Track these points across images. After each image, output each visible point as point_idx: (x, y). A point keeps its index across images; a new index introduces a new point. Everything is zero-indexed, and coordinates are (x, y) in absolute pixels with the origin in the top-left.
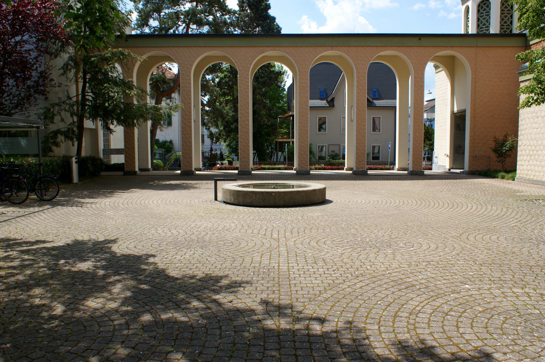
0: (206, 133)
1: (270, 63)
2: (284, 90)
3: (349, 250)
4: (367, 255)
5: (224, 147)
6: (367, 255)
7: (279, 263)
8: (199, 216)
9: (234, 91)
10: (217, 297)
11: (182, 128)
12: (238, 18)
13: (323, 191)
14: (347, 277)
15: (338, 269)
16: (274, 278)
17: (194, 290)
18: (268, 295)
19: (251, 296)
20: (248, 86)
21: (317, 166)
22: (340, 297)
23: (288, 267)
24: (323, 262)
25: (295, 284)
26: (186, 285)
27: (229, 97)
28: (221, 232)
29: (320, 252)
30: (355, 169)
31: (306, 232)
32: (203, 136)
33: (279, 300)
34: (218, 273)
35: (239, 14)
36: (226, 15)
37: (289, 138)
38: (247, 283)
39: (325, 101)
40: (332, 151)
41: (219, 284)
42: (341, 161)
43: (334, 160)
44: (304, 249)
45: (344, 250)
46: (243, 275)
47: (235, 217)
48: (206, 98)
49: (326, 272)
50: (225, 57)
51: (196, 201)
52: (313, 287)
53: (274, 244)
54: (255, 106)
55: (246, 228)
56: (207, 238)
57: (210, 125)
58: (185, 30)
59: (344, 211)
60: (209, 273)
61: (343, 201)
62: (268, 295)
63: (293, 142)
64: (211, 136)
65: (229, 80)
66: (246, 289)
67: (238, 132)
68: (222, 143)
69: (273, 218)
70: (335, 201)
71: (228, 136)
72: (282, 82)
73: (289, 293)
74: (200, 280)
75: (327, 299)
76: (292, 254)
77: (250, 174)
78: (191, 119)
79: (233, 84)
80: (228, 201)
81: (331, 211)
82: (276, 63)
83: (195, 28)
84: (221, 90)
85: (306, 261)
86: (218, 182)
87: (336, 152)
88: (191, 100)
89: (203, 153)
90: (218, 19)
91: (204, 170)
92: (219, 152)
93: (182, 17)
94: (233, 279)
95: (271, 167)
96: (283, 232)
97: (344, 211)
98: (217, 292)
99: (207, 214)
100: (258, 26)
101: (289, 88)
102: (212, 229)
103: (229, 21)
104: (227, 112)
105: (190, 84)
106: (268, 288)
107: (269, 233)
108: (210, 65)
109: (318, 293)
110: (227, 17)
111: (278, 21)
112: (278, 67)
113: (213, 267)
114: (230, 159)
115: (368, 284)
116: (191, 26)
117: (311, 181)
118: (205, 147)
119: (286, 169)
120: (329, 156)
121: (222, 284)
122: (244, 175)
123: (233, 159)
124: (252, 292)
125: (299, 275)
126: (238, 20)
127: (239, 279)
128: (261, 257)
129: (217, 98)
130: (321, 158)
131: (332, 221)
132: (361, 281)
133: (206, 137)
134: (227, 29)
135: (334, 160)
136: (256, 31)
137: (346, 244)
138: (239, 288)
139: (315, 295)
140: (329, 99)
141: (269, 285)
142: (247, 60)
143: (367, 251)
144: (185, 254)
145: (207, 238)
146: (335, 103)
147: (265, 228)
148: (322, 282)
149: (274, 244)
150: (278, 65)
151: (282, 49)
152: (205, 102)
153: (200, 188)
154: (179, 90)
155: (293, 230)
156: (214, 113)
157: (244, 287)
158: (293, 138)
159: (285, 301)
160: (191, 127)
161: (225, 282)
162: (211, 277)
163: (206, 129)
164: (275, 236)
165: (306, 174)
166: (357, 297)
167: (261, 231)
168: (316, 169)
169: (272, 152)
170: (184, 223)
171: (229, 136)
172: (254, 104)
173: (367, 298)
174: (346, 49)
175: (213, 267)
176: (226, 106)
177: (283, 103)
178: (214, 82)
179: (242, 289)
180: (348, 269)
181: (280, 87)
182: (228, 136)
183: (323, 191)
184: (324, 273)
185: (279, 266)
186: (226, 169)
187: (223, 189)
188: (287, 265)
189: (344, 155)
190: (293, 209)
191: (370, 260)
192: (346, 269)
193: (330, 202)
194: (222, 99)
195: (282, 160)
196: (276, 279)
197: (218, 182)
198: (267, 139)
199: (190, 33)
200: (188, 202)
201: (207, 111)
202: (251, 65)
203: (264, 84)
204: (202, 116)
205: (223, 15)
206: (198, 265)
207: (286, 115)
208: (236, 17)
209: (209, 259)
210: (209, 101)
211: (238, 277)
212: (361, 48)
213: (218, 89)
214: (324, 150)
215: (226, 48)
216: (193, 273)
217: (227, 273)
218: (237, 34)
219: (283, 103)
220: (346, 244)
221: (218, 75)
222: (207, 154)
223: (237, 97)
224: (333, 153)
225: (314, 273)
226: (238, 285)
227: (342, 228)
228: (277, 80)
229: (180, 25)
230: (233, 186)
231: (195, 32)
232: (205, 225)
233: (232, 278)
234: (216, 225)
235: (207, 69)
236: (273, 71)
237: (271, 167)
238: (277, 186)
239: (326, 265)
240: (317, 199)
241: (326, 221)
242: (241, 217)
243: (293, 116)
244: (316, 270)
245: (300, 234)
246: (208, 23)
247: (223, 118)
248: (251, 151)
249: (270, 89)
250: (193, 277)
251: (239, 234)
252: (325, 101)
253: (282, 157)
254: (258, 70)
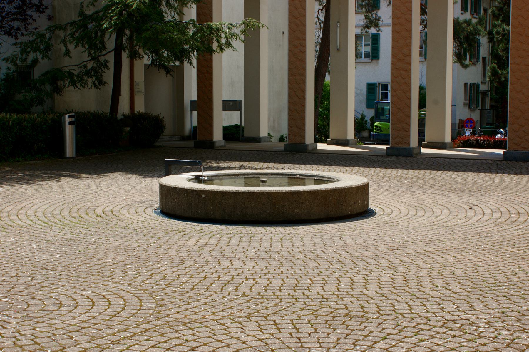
13: (362, 191)
183: (362, 191)
240: (350, 206)
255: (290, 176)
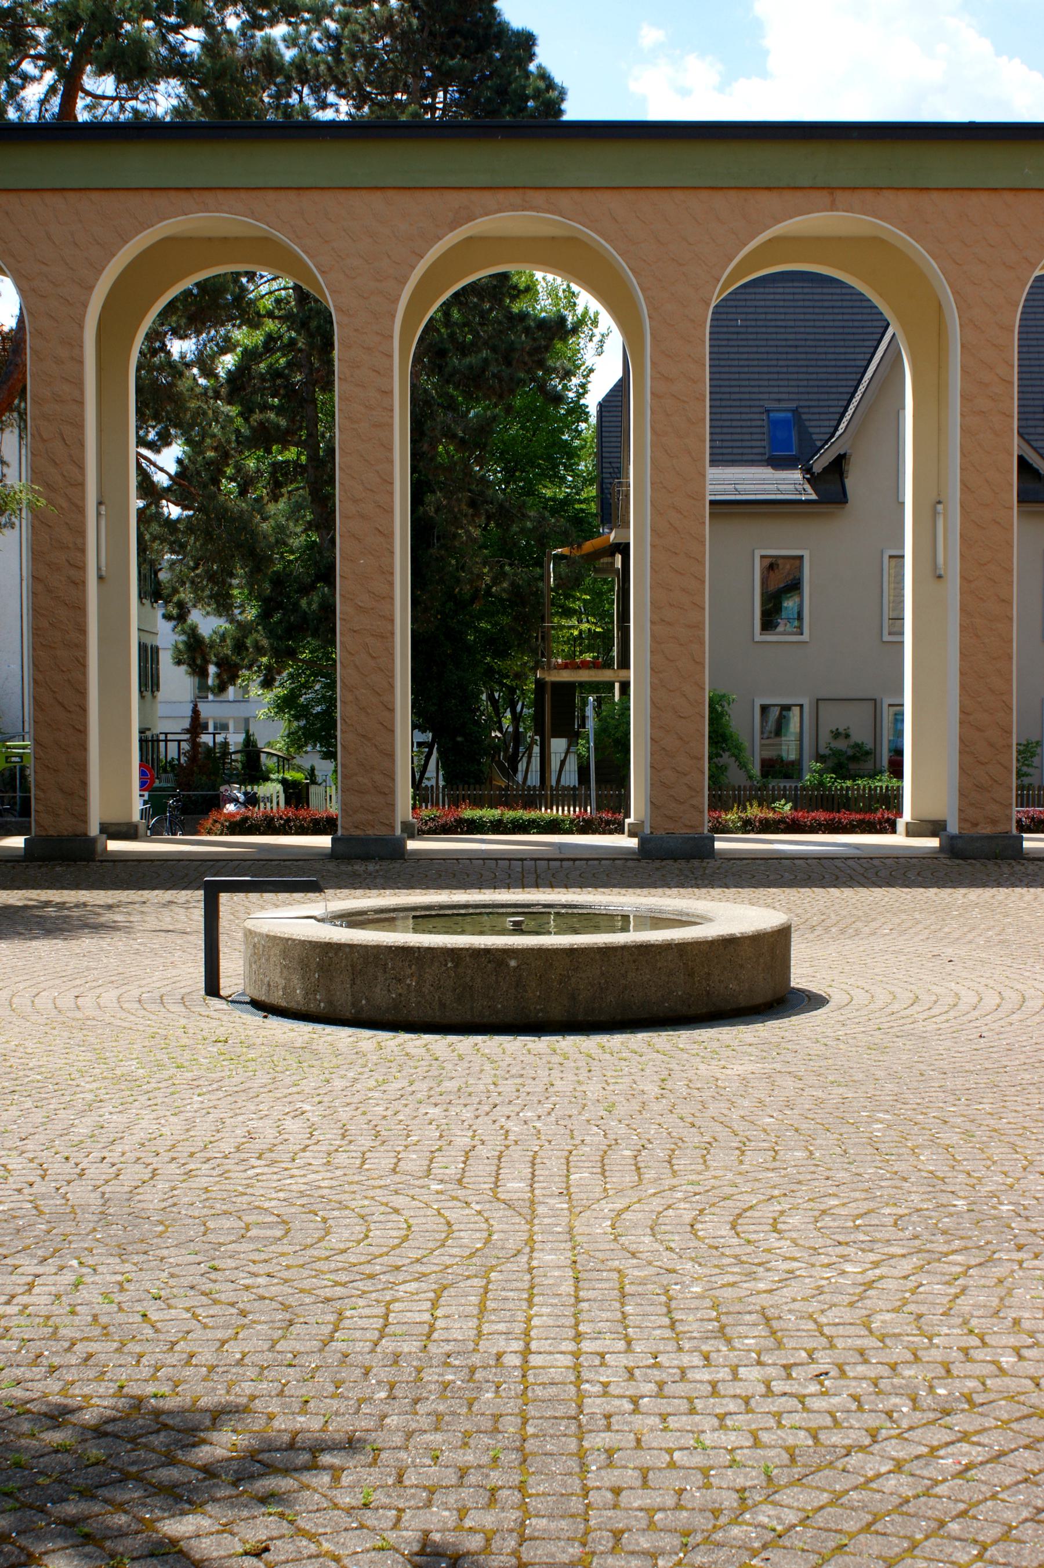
0: (167, 636)
1: (505, 276)
2: (579, 412)
3: (907, 1266)
4: (1001, 1291)
5: (261, 713)
6: (1001, 1291)
7: (527, 1333)
8: (118, 1079)
9: (316, 421)
10: (179, 1527)
11: (37, 611)
12: (337, 38)
13: (775, 945)
14: (889, 1414)
15: (841, 1368)
16: (497, 1418)
17: (66, 1486)
18: (462, 1512)
19: (370, 1518)
20: (390, 393)
21: (754, 812)
22: (851, 1526)
23: (576, 1355)
24: (761, 1330)
25: (610, 1452)
26: (24, 1458)
27: (291, 454)
28: (229, 1164)
29: (751, 1276)
30: (953, 828)
31: (680, 1164)
32: (149, 655)
33: (522, 1539)
34: (200, 1389)
35: (345, 20)
36: (273, 21)
37: (608, 665)
38: (351, 1445)
39: (797, 475)
40: (836, 735)
41: (204, 1454)
42: (884, 782)
43: (849, 783)
44: (667, 1259)
45: (876, 1265)
46: (335, 1404)
47: (309, 1085)
48: (168, 460)
49: (778, 1386)
50: (266, 241)
51: (109, 996)
52: (705, 1472)
53: (509, 1230)
54: (430, 498)
55: (365, 1142)
56: (152, 1198)
57: (186, 595)
58: (56, 101)
59: (884, 1050)
60: (150, 1389)
61: (882, 997)
62: (462, 1512)
63: (625, 687)
64: (194, 653)
65: (289, 364)
66: (346, 1479)
67: (333, 631)
68: (255, 690)
69: (508, 1087)
70: (837, 997)
71: (284, 654)
72: (568, 374)
73: (576, 1505)
74: (98, 1432)
75: (777, 1538)
76: (600, 1288)
77: (398, 852)
78: (82, 568)
79: (310, 383)
80: (277, 998)
81: (816, 1049)
82: (539, 275)
83: (110, 91)
84: (245, 415)
85: (673, 1324)
86: (224, 898)
87: (857, 737)
88: (81, 468)
89: (149, 743)
90: (233, 44)
91: (155, 832)
92: (235, 739)
93: (41, 34)
94: (278, 1424)
95: (510, 814)
96: (554, 1165)
97: (884, 1050)
98: (181, 1498)
99: (160, 1066)
100: (443, 79)
101: (603, 406)
102: (182, 1151)
103: (289, 55)
104: (280, 529)
105: (79, 384)
106: (463, 1473)
107: (481, 1171)
108: (188, 283)
109: (730, 1500)
110: (280, 31)
111: (548, 57)
112: (553, 293)
113: (171, 1359)
114: (299, 776)
115: (1002, 1454)
116: (89, 82)
117: (716, 892)
118: (161, 710)
119: (587, 827)
120: (820, 758)
121: (220, 1452)
122: (366, 858)
123: (312, 773)
124: (379, 1497)
125: (635, 1400)
126: (336, 52)
127: (309, 1424)
128: (435, 1304)
129: (226, 456)
130: (776, 768)
131: (819, 1102)
132: (964, 1437)
133: (166, 659)
134: (277, 96)
135: (849, 783)
136: (432, 108)
137: (889, 1233)
138: (306, 1477)
139: (716, 1513)
140: (819, 463)
141: (469, 1457)
142: (382, 260)
143: (998, 1271)
144: (31, 1286)
145: (152, 1198)
146: (848, 482)
147: (463, 1141)
148: (757, 1443)
149: (509, 1230)
150: (548, 287)
151: (564, 200)
152: (162, 480)
153: (127, 929)
154: (22, 416)
155: (613, 1157)
156: (209, 537)
157: (336, 1472)
158: (625, 664)
159: (551, 1547)
160: (81, 608)
161: (223, 1444)
162: (157, 1413)
163: (167, 617)
164: (515, 1186)
165: (689, 857)
166: (942, 1524)
167: (440, 1160)
168: (748, 826)
169: (517, 737)
170: (38, 1117)
171: (292, 653)
172: (419, 491)
173: (996, 1531)
174: (904, 201)
175: (171, 1359)
176: (275, 498)
177: (575, 485)
178: (208, 372)
179: (326, 1478)
180: (893, 1367)
181: (558, 399)
182: (284, 654)
183: (775, 945)
184: (769, 1392)
185: (526, 1352)
186: (270, 827)
187: (249, 933)
188: (570, 1346)
189: (899, 752)
190: (616, 1041)
191: (1017, 1322)
192: (885, 1371)
193: (812, 1001)
194: (252, 464)
195: (570, 778)
196: (510, 1426)
197: (224, 898)
198: (490, 671)
199: (83, 116)
200: (66, 1001)
201: (170, 524)
202: (403, 281)
203: (474, 382)
204: (142, 549)
205: (256, 23)
206: (93, 1347)
207: (588, 546)
208: (328, 35)
209: (154, 1316)
210: (183, 473)
211: (303, 1412)
212: (984, 197)
213: (232, 410)
214: (794, 725)
215: (271, 195)
216: (64, 1392)
217: (248, 1388)
218: (332, 125)
219: (575, 485)
220: (889, 1233)
221: (227, 339)
222: (173, 747)
223: (331, 451)
224: (841, 745)
225: (715, 1392)
226: (304, 1457)
227: (872, 1141)
228: (541, 364)
229: (26, 78)
230: (299, 918)
231: (110, 112)
232: (147, 1124)
233: (271, 1417)
234: (203, 1130)
235: (171, 304)
236: (523, 316)
237: (510, 814)
238: (532, 918)
239: (779, 1345)
240: (747, 987)
241: (789, 1105)
242: (338, 1084)
243: (623, 549)
244: (724, 1374)
245: (649, 1175)
246: (178, 67)
247: (256, 558)
248: (405, 738)
249: (509, 409)
250: (58, 1416)
251: (322, 1178)
252: (797, 475)
253: (572, 765)
254: (447, 306)
255: (418, 914)
